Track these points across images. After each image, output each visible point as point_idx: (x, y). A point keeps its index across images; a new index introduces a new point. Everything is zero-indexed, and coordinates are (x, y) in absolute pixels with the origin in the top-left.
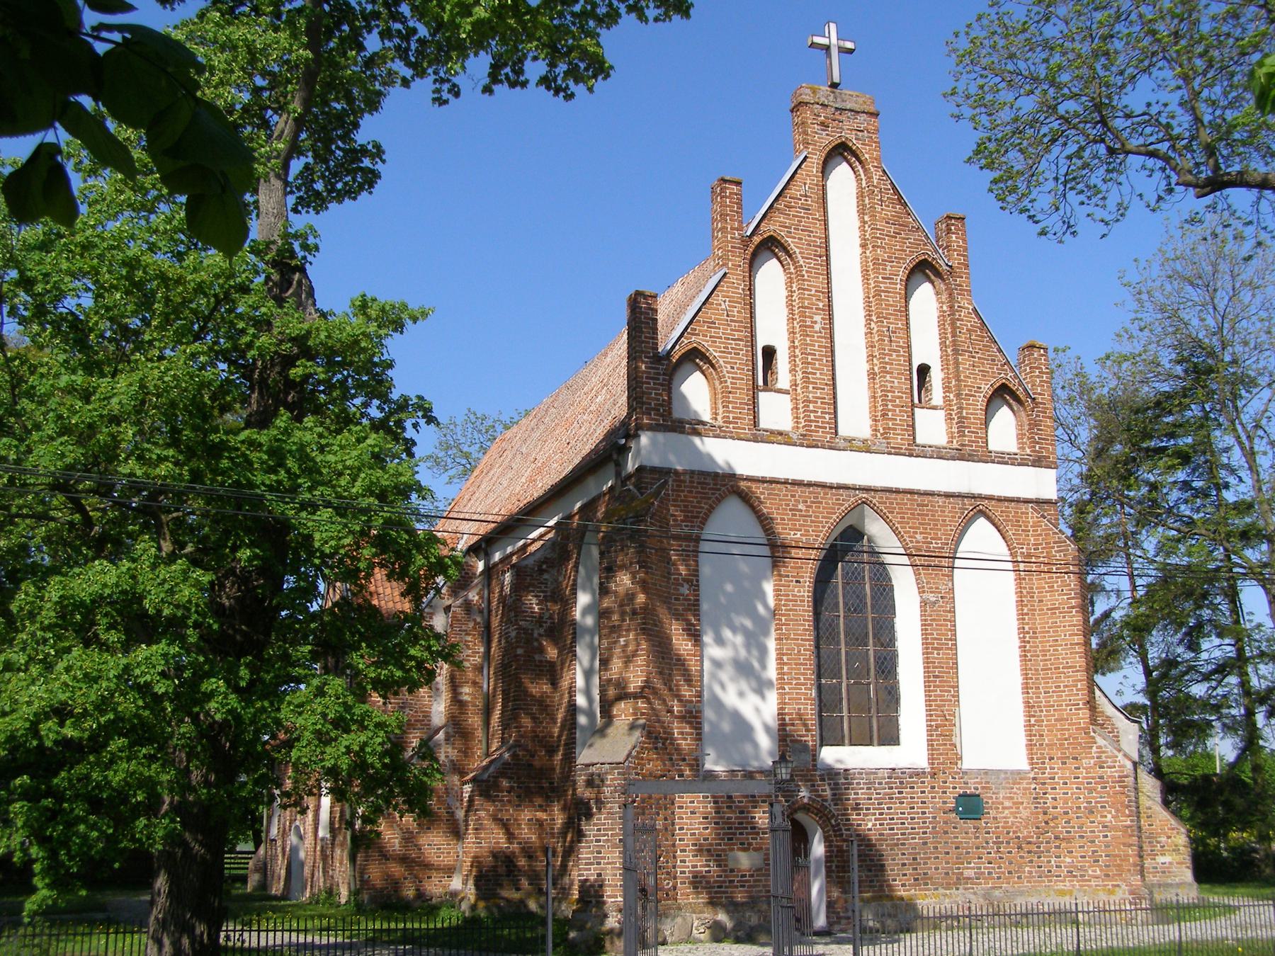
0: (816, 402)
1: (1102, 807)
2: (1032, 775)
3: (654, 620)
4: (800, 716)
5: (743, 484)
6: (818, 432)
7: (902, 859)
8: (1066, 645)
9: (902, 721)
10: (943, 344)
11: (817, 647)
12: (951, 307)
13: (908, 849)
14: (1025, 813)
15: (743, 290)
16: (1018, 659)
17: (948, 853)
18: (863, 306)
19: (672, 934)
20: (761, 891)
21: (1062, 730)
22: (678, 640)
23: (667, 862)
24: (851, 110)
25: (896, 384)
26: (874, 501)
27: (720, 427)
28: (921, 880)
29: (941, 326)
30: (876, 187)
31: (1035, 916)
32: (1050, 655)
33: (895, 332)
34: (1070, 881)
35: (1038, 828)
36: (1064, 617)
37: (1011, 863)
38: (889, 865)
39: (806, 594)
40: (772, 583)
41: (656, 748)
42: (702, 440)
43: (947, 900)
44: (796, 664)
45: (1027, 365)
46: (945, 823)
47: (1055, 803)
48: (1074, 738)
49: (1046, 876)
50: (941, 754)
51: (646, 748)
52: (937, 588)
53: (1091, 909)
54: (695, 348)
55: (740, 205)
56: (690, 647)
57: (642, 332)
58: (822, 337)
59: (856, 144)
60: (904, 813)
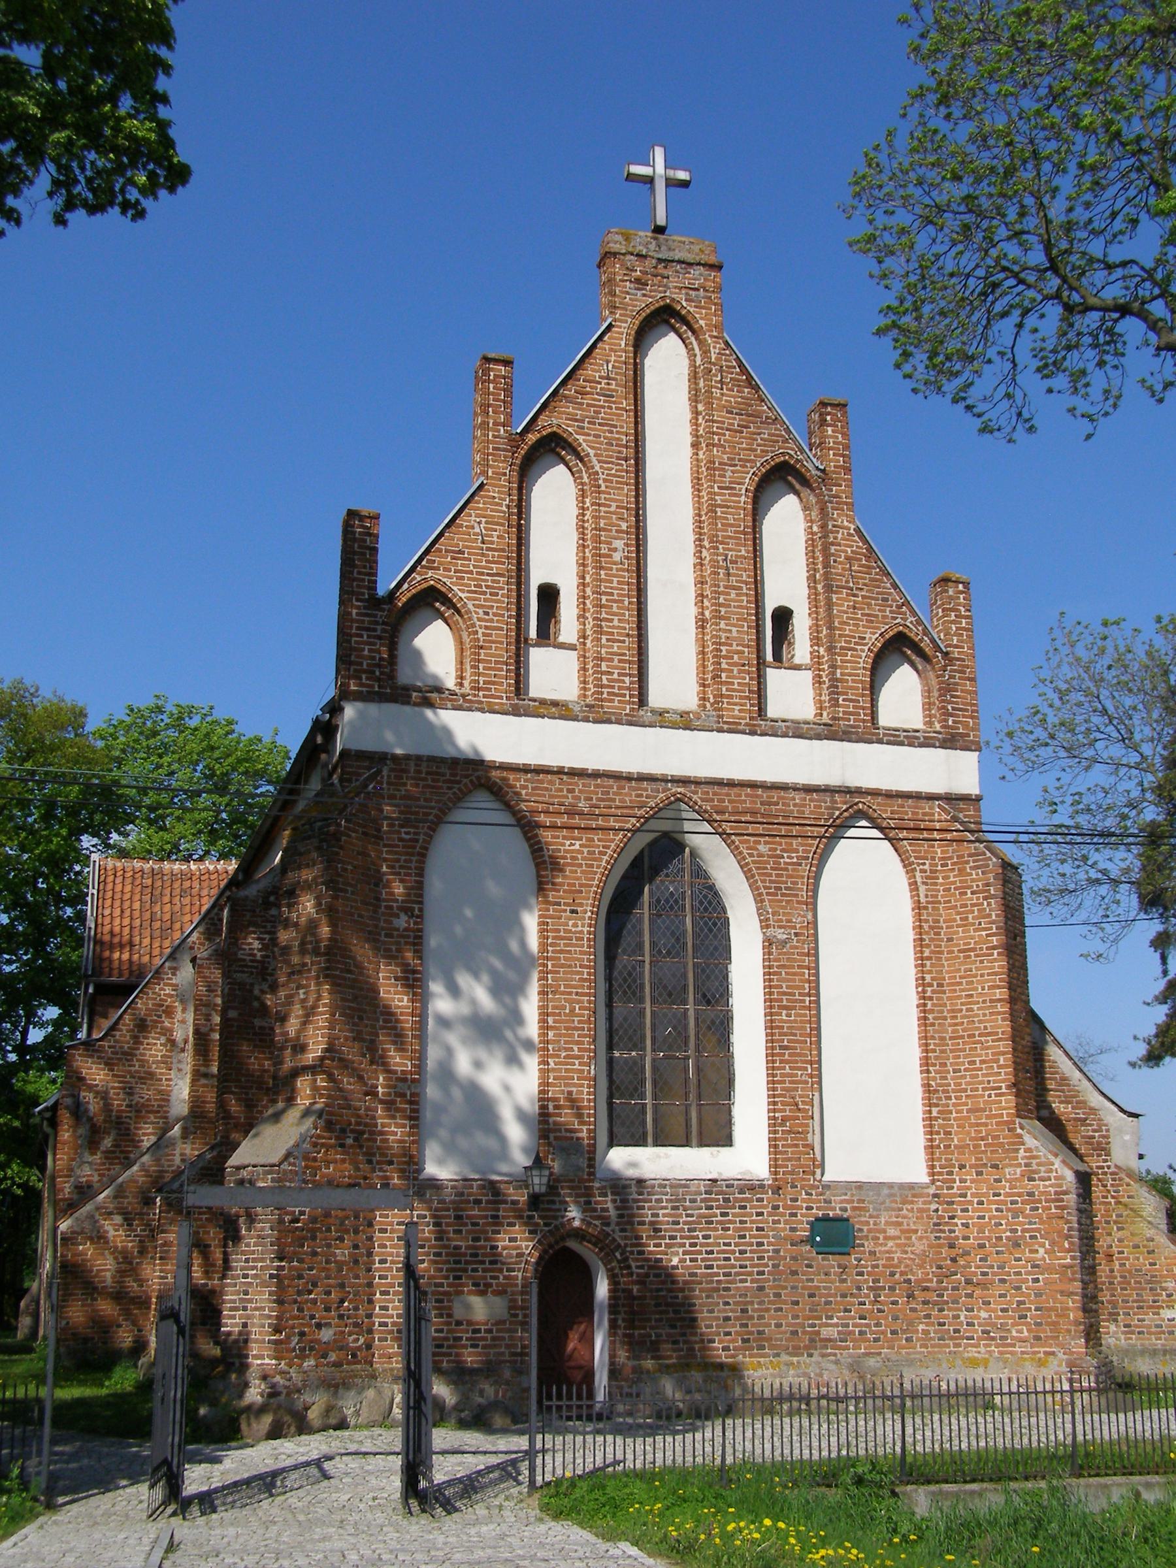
0: (612, 660)
1: (1031, 1237)
2: (932, 1191)
3: (345, 963)
4: (572, 1101)
5: (494, 774)
6: (612, 701)
7: (725, 1311)
8: (984, 1001)
9: (736, 1111)
10: (812, 579)
11: (609, 1005)
12: (823, 527)
13: (734, 1296)
14: (919, 1247)
15: (508, 507)
16: (916, 1023)
17: (797, 1303)
18: (692, 527)
19: (357, 1413)
20: (502, 1354)
21: (978, 1125)
22: (389, 992)
23: (356, 1309)
24: (680, 262)
25: (735, 634)
26: (695, 797)
27: (463, 696)
28: (756, 1341)
29: (810, 554)
30: (714, 364)
31: (1041, 1397)
32: (962, 1017)
33: (736, 562)
34: (986, 1346)
35: (939, 1267)
36: (982, 962)
37: (895, 1318)
38: (703, 1319)
39: (586, 929)
40: (537, 914)
41: (342, 1146)
42: (435, 714)
43: (792, 1372)
44: (567, 1029)
45: (938, 608)
46: (794, 1258)
47: (966, 1232)
48: (994, 1137)
49: (951, 1338)
50: (789, 1159)
51: (323, 1145)
52: (789, 921)
53: (1014, 1389)
54: (432, 588)
55: (508, 391)
56: (405, 1003)
57: (354, 566)
58: (623, 570)
59: (686, 306)
60: (729, 1244)
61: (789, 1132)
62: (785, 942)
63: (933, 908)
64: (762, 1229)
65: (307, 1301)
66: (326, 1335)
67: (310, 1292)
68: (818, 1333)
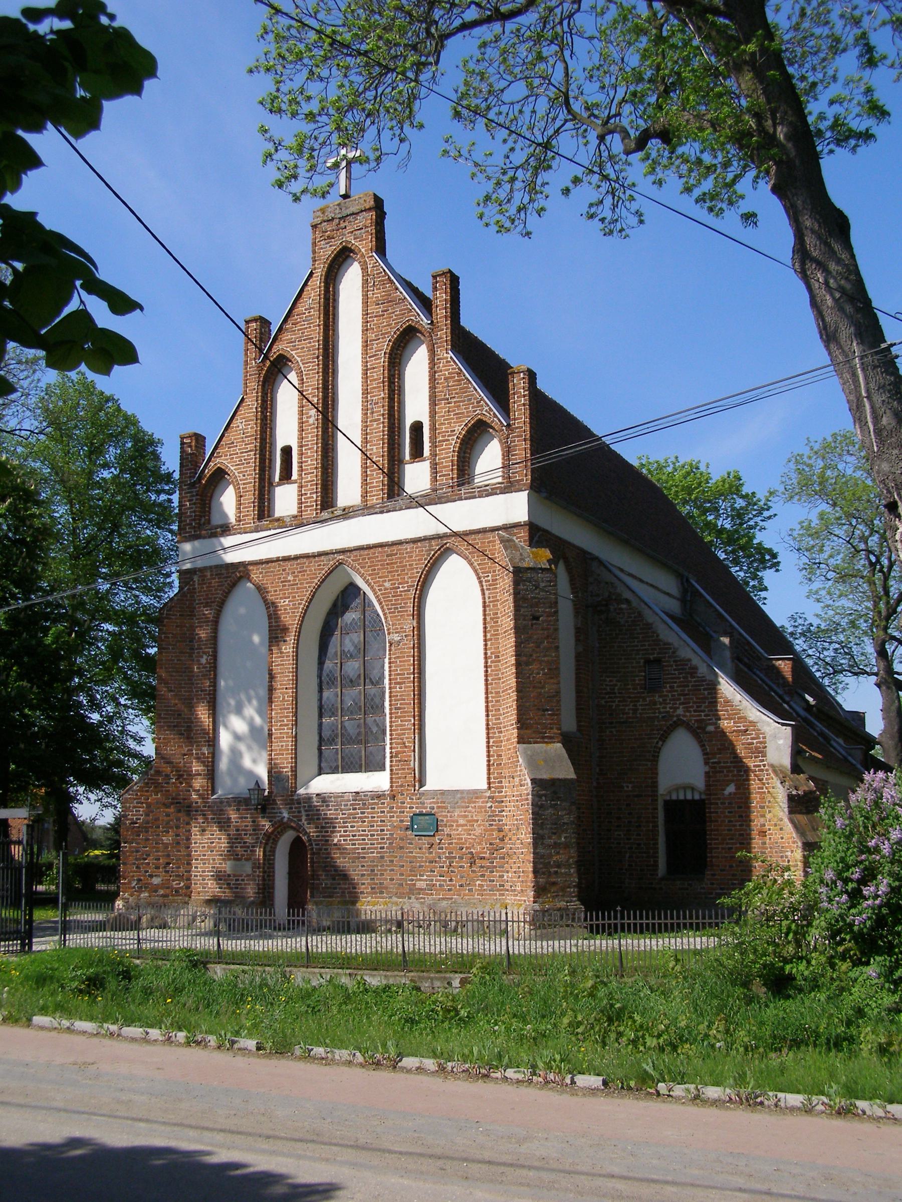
2: (488, 794)
13: (367, 862)
14: (478, 831)
25: (375, 451)
35: (491, 844)
46: (401, 839)
49: (498, 890)
50: (399, 778)
61: (400, 761)
62: (399, 642)
63: (494, 606)
64: (384, 821)
65: (142, 864)
66: (156, 881)
67: (145, 859)
68: (415, 885)
